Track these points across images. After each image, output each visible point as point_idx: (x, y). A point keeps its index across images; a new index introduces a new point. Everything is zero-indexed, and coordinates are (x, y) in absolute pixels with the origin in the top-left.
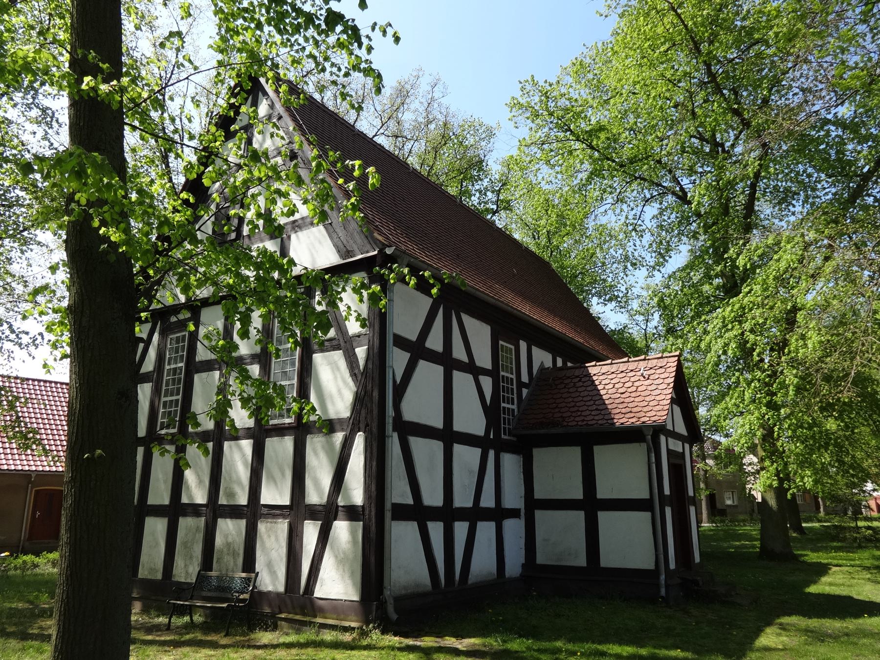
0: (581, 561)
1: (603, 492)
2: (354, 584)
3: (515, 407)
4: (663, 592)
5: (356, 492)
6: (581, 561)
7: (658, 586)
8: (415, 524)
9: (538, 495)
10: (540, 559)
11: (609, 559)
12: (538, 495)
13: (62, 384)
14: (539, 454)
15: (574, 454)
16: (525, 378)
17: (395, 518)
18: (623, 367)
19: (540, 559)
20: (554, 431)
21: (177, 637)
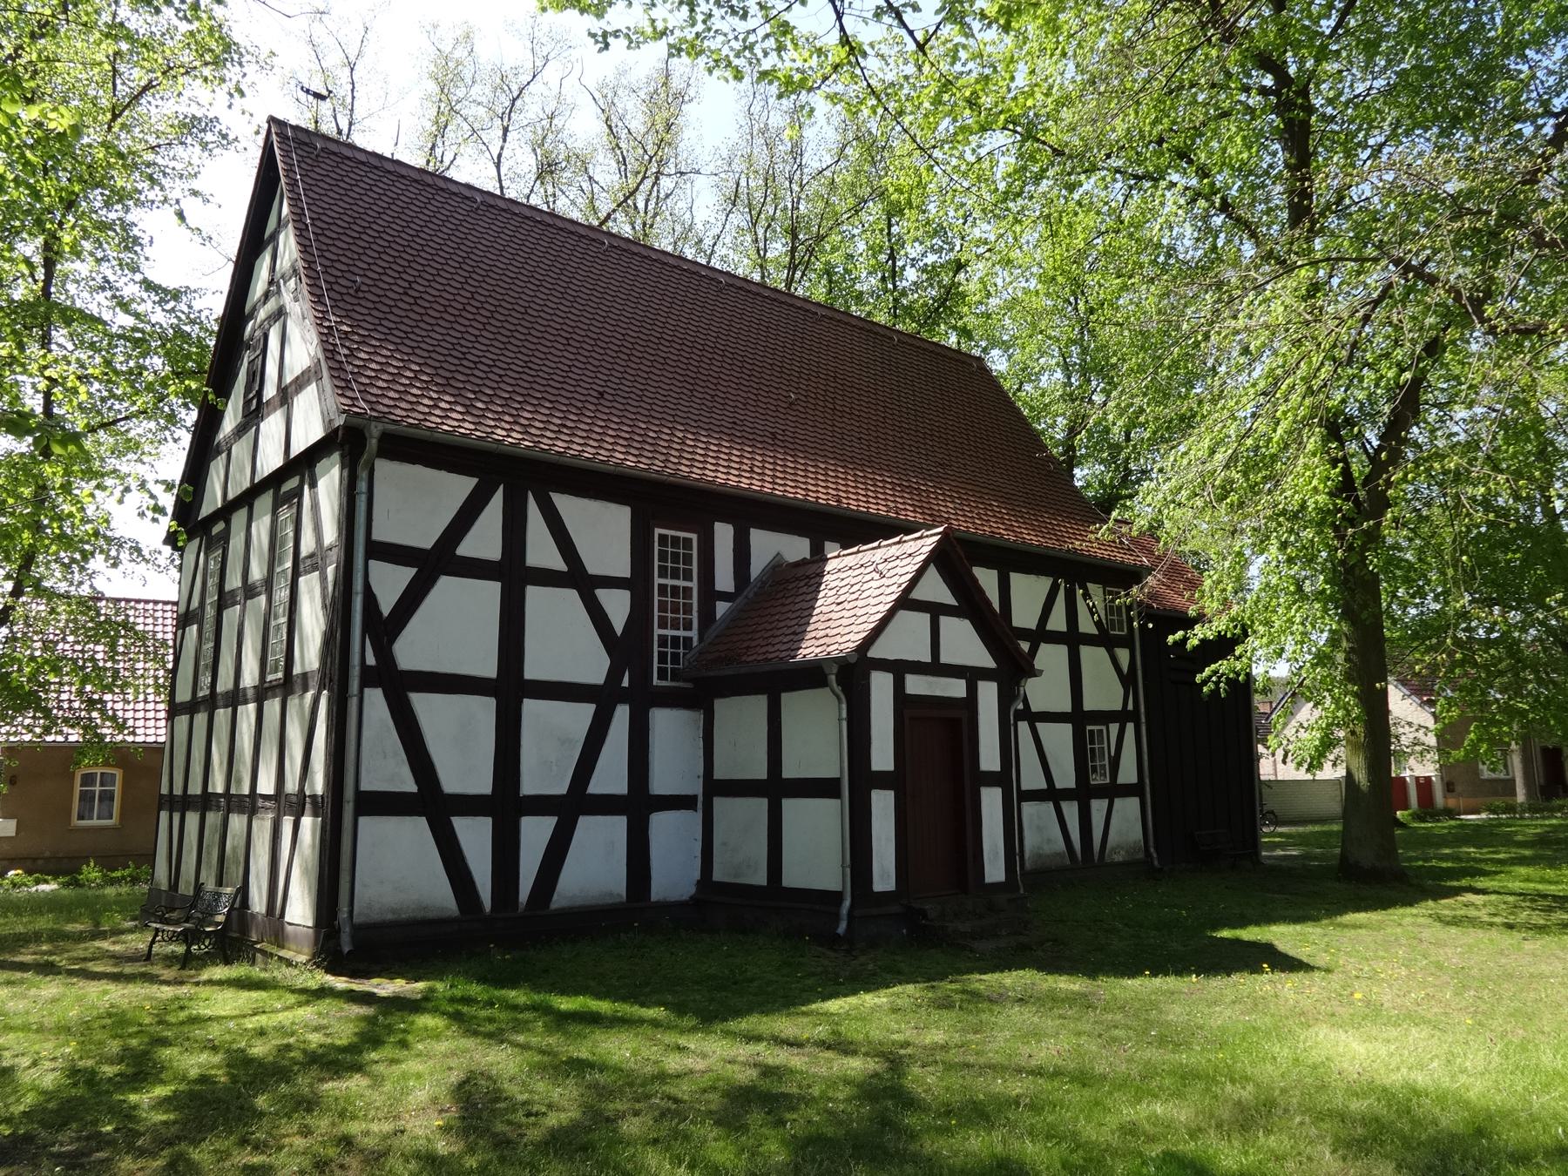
0: (760, 878)
1: (760, 772)
2: (307, 900)
3: (694, 634)
4: (842, 928)
5: (318, 784)
6: (760, 878)
7: (836, 918)
8: (423, 821)
9: (719, 774)
10: (718, 875)
11: (792, 877)
12: (719, 774)
13: (166, 603)
14: (787, 699)
15: (759, 703)
16: (724, 579)
17: (695, 797)
18: (894, 551)
19: (718, 875)
20: (729, 671)
21: (465, 1009)
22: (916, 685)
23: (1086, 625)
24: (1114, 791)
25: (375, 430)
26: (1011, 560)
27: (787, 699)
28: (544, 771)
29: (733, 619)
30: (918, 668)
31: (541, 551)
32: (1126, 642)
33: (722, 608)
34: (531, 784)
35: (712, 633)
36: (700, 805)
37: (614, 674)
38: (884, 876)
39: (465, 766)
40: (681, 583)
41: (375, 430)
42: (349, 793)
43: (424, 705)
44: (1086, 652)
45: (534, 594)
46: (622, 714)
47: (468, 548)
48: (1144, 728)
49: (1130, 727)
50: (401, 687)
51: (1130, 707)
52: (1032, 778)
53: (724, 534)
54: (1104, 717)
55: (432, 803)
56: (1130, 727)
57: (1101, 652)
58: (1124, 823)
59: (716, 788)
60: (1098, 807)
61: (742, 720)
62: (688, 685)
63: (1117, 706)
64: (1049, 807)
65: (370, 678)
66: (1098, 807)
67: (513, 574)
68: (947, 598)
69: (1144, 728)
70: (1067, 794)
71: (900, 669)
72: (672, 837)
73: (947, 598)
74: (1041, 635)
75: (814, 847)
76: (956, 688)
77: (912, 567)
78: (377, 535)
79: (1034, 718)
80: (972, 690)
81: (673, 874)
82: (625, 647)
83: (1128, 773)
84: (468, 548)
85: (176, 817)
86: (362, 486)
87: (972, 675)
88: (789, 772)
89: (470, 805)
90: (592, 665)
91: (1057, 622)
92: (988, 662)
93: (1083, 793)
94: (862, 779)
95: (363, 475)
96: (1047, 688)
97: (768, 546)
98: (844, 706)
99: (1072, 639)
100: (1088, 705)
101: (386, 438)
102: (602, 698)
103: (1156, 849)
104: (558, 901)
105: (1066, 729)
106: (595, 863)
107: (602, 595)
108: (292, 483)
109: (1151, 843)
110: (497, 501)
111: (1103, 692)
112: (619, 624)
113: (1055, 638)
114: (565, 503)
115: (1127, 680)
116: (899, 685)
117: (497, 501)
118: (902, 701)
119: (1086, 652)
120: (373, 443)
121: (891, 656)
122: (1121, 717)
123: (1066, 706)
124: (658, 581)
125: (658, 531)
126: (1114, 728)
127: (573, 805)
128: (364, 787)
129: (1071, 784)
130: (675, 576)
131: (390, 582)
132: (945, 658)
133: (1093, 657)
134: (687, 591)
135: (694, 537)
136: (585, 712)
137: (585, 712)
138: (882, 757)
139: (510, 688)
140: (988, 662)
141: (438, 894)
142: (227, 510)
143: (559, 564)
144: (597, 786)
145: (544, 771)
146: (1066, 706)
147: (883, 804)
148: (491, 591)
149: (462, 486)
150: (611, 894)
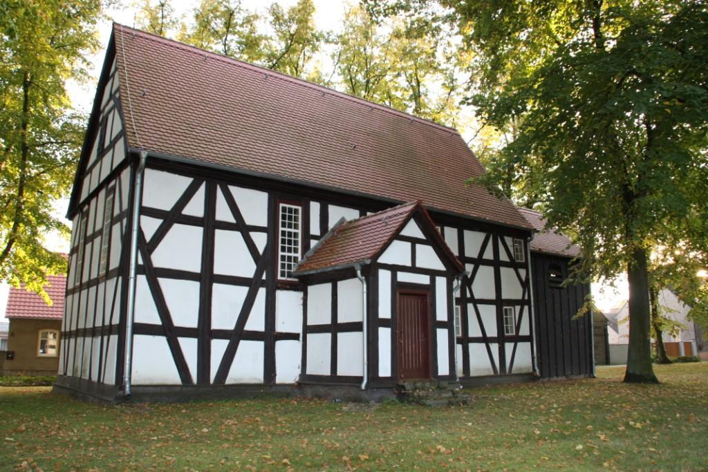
0: (327, 372)
3: (299, 255)
9: (309, 323)
12: (309, 323)
14: (340, 284)
15: (328, 287)
16: (315, 229)
19: (309, 372)
22: (403, 277)
23: (503, 257)
24: (517, 339)
25: (144, 155)
26: (463, 223)
27: (340, 284)
28: (224, 315)
29: (318, 250)
30: (404, 269)
31: (223, 213)
32: (525, 266)
33: (313, 243)
34: (216, 325)
35: (309, 254)
36: (301, 338)
37: (258, 273)
38: (385, 370)
39: (185, 313)
40: (293, 230)
41: (144, 155)
42: (129, 324)
43: (164, 283)
44: (503, 270)
45: (219, 233)
46: (262, 292)
47: (188, 210)
48: (533, 308)
49: (526, 308)
50: (154, 275)
51: (526, 297)
52: (474, 331)
53: (315, 207)
54: (512, 303)
55: (168, 330)
56: (526, 308)
57: (511, 271)
58: (523, 357)
59: (308, 329)
60: (509, 347)
61: (320, 294)
62: (296, 280)
63: (519, 297)
64: (483, 345)
65: (139, 270)
66: (509, 347)
67: (209, 224)
68: (421, 235)
69: (533, 308)
70: (493, 340)
71: (394, 269)
72: (287, 354)
73: (421, 235)
74: (479, 262)
75: (352, 362)
76: (424, 280)
77: (401, 219)
78: (145, 204)
79: (476, 302)
80: (433, 281)
81: (287, 372)
82: (265, 261)
83: (524, 331)
84: (188, 210)
85: (67, 341)
86: (138, 181)
87: (433, 274)
88: (341, 320)
89: (187, 332)
90: (248, 269)
91: (489, 255)
92: (442, 267)
93: (501, 339)
94: (374, 322)
95: (139, 176)
96: (483, 285)
97: (337, 214)
98: (365, 286)
99: (496, 264)
100: (504, 296)
101: (149, 158)
102: (252, 284)
103: (538, 367)
104: (230, 380)
105: (493, 308)
106: (248, 365)
107: (253, 235)
108: (112, 183)
109: (536, 364)
110: (202, 190)
111: (512, 290)
112: (261, 249)
113: (487, 263)
114: (234, 190)
115: (525, 285)
116: (394, 277)
117: (202, 190)
118: (397, 287)
119: (503, 270)
120: (143, 161)
121: (390, 262)
122: (522, 303)
123: (493, 296)
124: (281, 229)
125: (281, 205)
126: (518, 308)
127: (238, 335)
128: (137, 321)
129: (495, 335)
130: (290, 226)
131: (150, 226)
132: (418, 265)
133: (507, 274)
134: (296, 235)
135: (300, 208)
136: (244, 291)
137: (244, 291)
138: (385, 311)
139: (207, 278)
140: (442, 267)
141: (171, 375)
142: (88, 201)
143: (232, 220)
144: (250, 326)
145: (224, 315)
146: (493, 296)
147: (385, 334)
148: (198, 231)
149: (186, 181)
150: (256, 379)
